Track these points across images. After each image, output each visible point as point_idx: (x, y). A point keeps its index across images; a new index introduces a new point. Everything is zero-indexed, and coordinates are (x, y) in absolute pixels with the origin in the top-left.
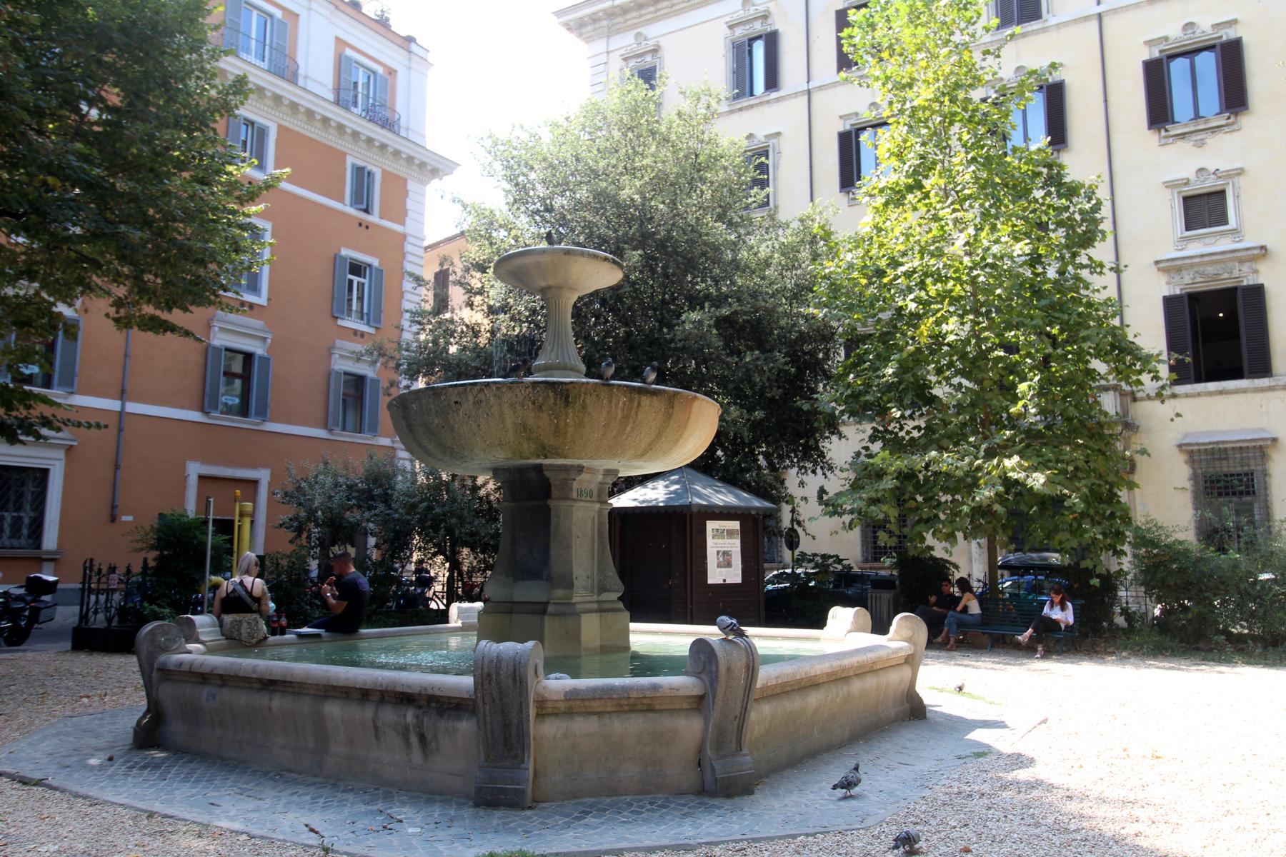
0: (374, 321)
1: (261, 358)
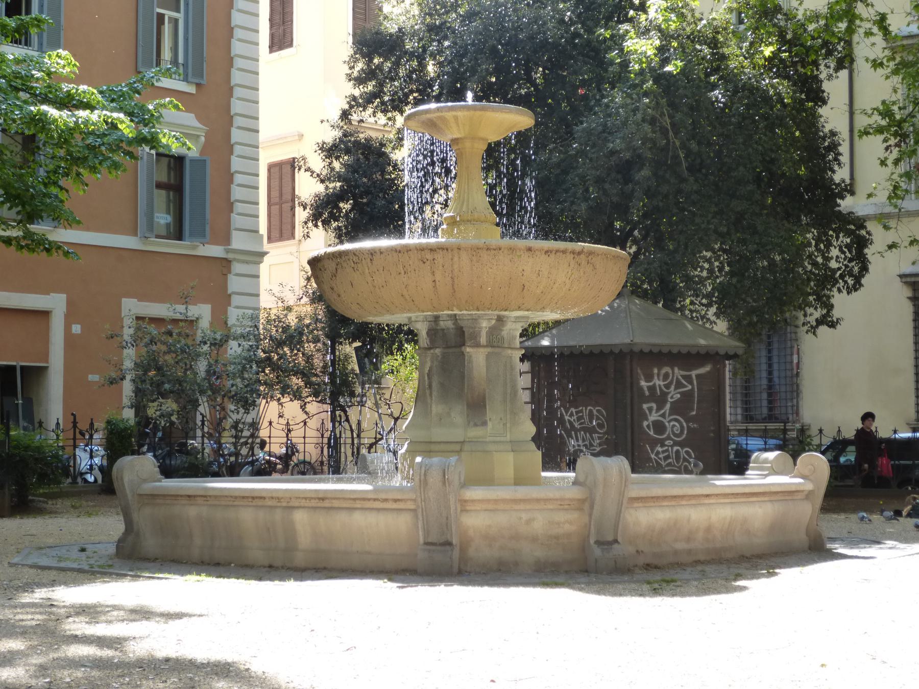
0: (194, 75)
1: (193, 161)
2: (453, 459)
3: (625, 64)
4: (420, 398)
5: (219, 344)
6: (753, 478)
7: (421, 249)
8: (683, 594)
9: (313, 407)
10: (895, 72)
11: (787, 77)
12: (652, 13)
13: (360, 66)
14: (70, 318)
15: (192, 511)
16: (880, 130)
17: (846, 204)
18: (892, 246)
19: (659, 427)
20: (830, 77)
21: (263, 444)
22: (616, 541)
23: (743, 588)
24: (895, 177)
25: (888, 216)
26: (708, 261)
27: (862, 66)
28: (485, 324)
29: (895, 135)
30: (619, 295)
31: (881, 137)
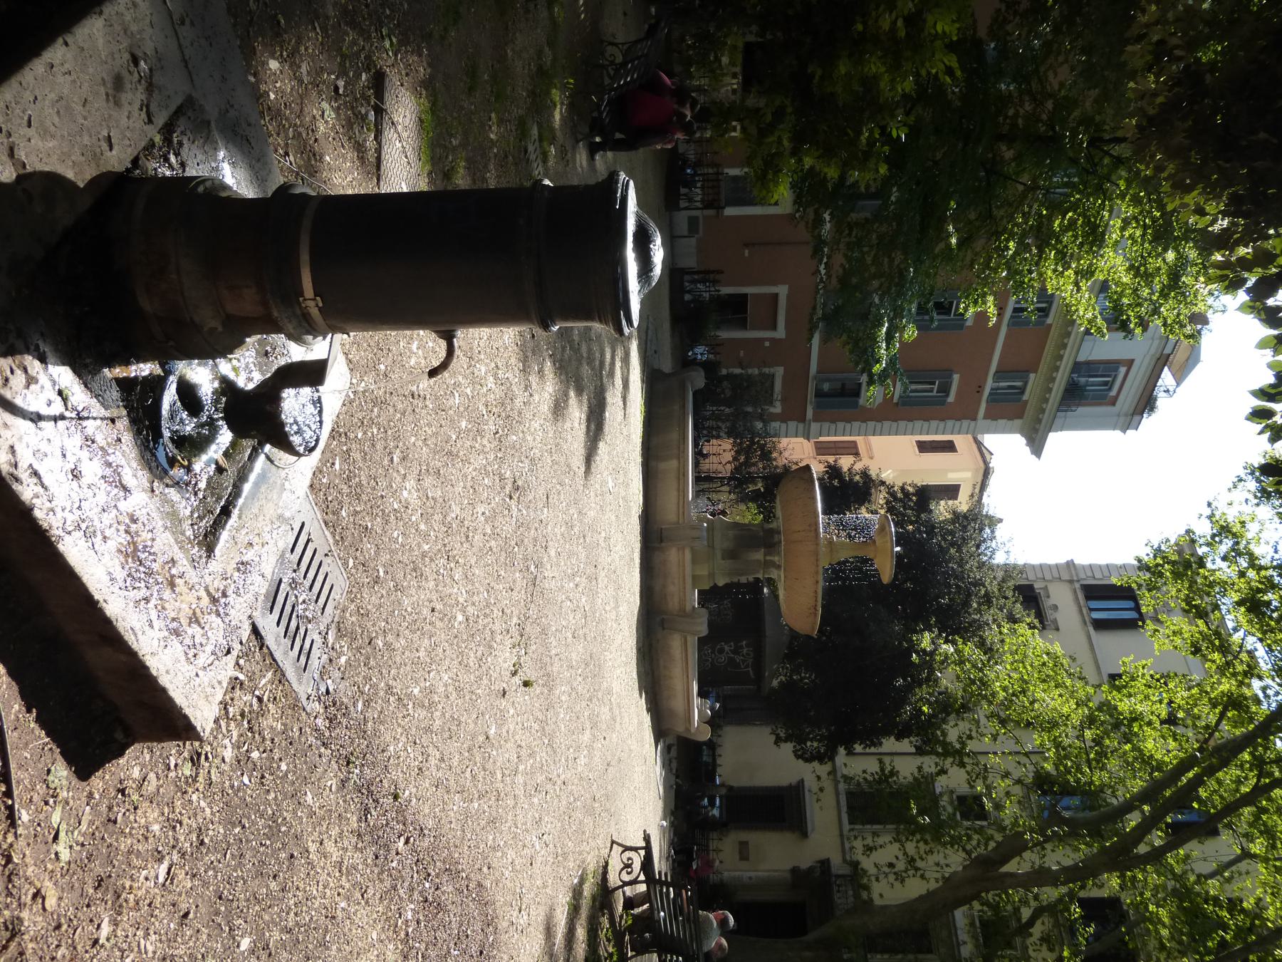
1: (857, 402)
2: (705, 543)
3: (916, 632)
4: (736, 525)
5: (761, 418)
6: (696, 701)
7: (817, 524)
8: (638, 664)
9: (729, 467)
10: (915, 779)
11: (911, 719)
12: (944, 646)
13: (911, 490)
14: (772, 340)
15: (676, 407)
16: (882, 769)
17: (842, 751)
18: (819, 778)
19: (721, 651)
20: (911, 742)
21: (709, 441)
22: (664, 629)
23: (641, 697)
24: (857, 778)
25: (835, 776)
26: (810, 677)
27: (918, 760)
28: (776, 559)
29: (880, 778)
30: (791, 629)
31: (878, 771)
